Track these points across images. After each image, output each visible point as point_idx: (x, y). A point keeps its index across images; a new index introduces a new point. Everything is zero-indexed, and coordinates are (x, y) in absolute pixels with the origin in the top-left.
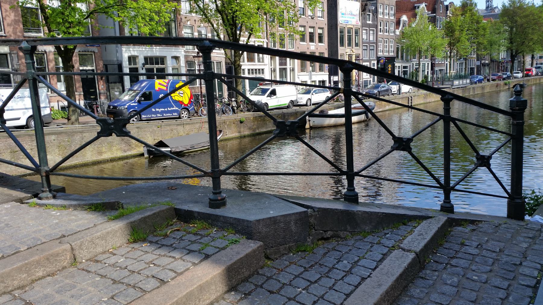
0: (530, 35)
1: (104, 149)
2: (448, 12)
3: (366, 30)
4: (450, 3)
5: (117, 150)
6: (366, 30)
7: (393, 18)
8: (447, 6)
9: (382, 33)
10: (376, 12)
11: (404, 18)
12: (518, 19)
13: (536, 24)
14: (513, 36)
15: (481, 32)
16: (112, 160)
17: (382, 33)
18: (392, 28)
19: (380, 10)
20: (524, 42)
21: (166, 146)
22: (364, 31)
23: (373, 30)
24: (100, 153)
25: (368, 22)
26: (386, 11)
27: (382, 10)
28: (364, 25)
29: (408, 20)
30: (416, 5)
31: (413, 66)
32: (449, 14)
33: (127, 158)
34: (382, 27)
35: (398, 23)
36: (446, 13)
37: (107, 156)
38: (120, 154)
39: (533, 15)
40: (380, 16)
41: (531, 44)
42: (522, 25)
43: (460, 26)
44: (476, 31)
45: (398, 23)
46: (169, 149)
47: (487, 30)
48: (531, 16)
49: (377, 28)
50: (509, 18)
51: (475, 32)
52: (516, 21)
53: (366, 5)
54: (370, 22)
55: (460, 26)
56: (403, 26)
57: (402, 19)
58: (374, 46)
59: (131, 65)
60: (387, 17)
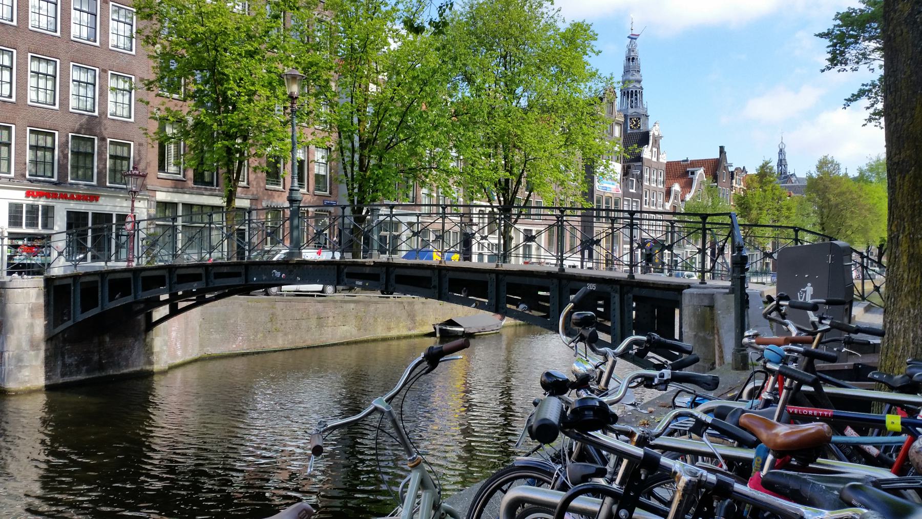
0: (848, 221)
1: (392, 325)
2: (734, 181)
3: (628, 201)
4: (736, 169)
5: (403, 327)
6: (628, 200)
7: (661, 186)
8: (732, 173)
9: (647, 206)
10: (640, 178)
11: (676, 187)
12: (831, 197)
13: (855, 205)
14: (824, 220)
15: (785, 212)
16: (399, 338)
17: (647, 206)
18: (661, 201)
19: (646, 176)
20: (840, 229)
21: (457, 325)
22: (626, 203)
23: (637, 202)
24: (389, 329)
25: (631, 191)
26: (654, 177)
27: (648, 176)
28: (626, 194)
29: (682, 191)
30: (688, 169)
31: (687, 254)
32: (734, 184)
33: (410, 337)
34: (647, 198)
35: (668, 193)
36: (732, 183)
37: (394, 333)
38: (405, 332)
39: (851, 192)
40: (646, 183)
41: (849, 233)
42: (837, 205)
43: (757, 203)
44: (778, 210)
45: (668, 193)
46: (462, 329)
47: (793, 211)
48: (848, 194)
49: (641, 199)
50: (819, 195)
51: (777, 213)
52: (829, 200)
53: (629, 167)
54: (633, 191)
55: (757, 203)
56: (675, 198)
57: (673, 189)
58: (52, 177)
59: (19, 224)
60: (654, 185)
